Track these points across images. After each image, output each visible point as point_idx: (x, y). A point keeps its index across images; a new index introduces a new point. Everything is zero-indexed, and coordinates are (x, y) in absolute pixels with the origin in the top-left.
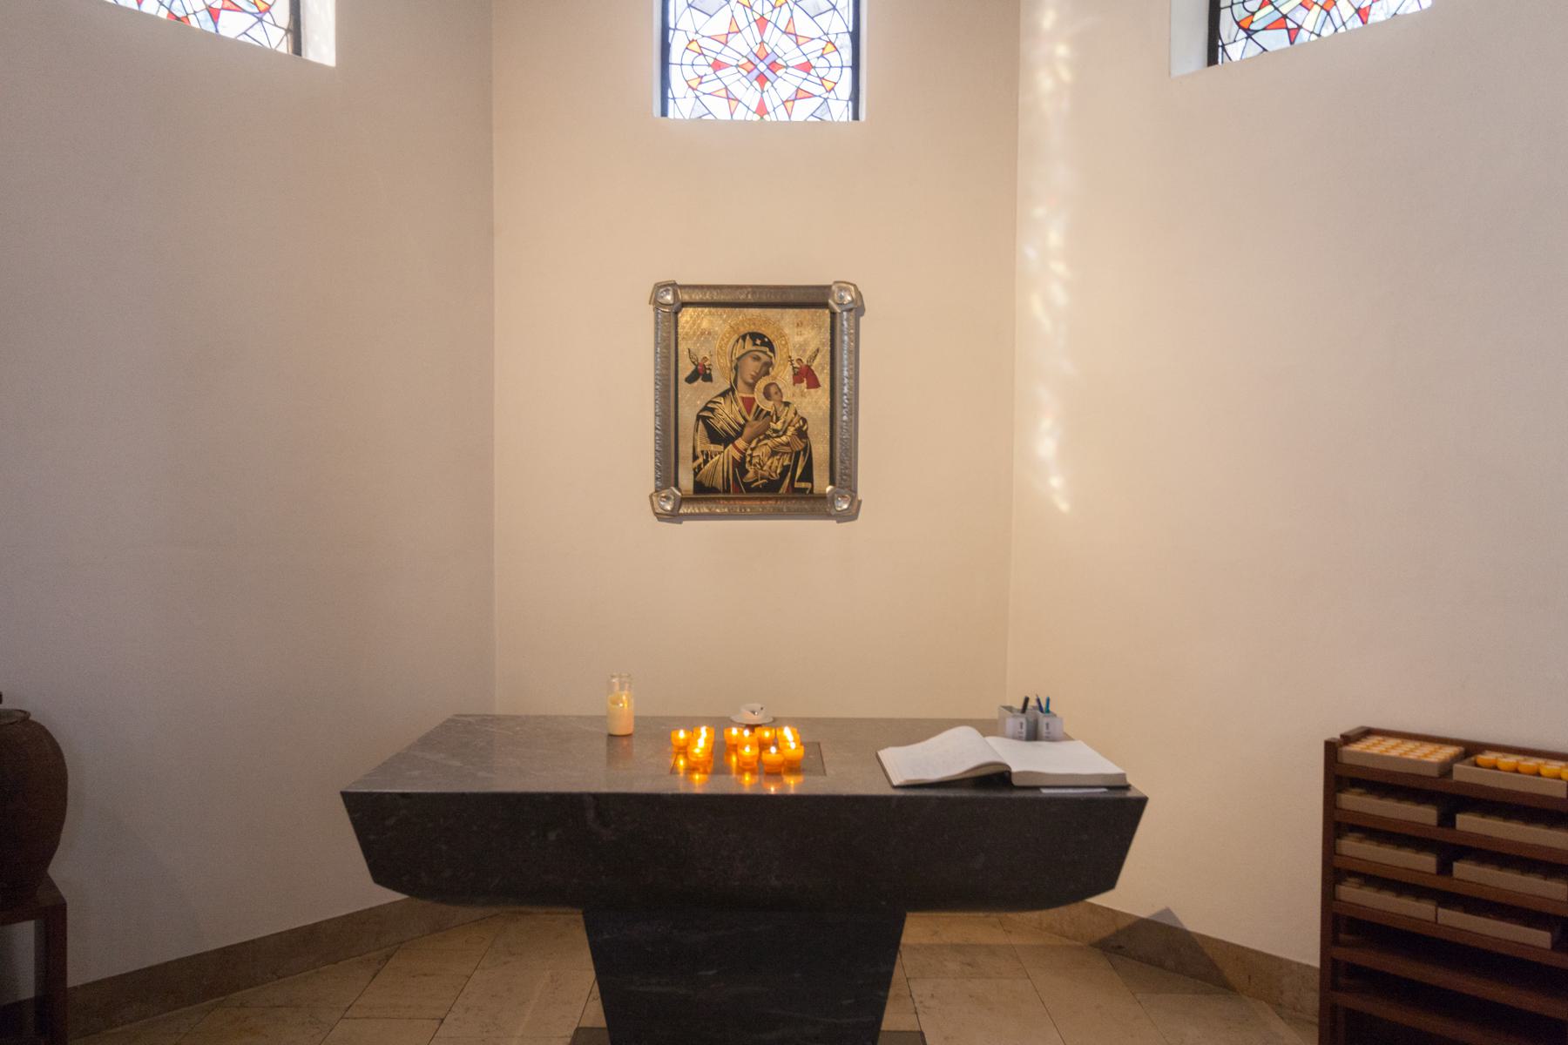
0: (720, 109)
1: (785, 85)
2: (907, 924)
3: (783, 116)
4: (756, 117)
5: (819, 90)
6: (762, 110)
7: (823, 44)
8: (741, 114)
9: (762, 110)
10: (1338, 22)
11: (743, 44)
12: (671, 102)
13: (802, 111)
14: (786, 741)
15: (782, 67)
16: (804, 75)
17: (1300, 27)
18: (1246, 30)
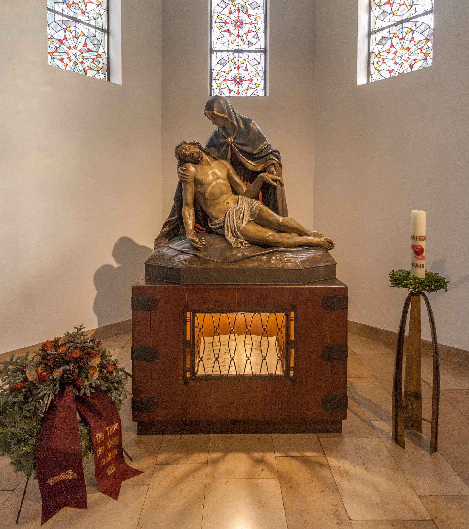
0: (226, 93)
1: (246, 84)
2: (115, 82)
3: (245, 95)
4: (237, 95)
5: (255, 30)
6: (239, 93)
7: (255, 73)
8: (232, 94)
9: (239, 93)
10: (404, 70)
11: (234, 16)
12: (213, 33)
13: (250, 93)
14: (188, 225)
15: (244, 80)
16: (250, 82)
17: (394, 2)
18: (378, 6)
